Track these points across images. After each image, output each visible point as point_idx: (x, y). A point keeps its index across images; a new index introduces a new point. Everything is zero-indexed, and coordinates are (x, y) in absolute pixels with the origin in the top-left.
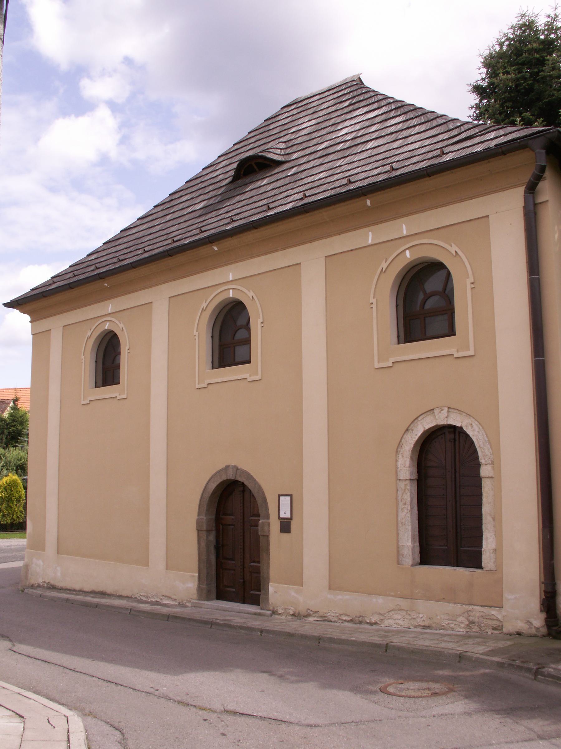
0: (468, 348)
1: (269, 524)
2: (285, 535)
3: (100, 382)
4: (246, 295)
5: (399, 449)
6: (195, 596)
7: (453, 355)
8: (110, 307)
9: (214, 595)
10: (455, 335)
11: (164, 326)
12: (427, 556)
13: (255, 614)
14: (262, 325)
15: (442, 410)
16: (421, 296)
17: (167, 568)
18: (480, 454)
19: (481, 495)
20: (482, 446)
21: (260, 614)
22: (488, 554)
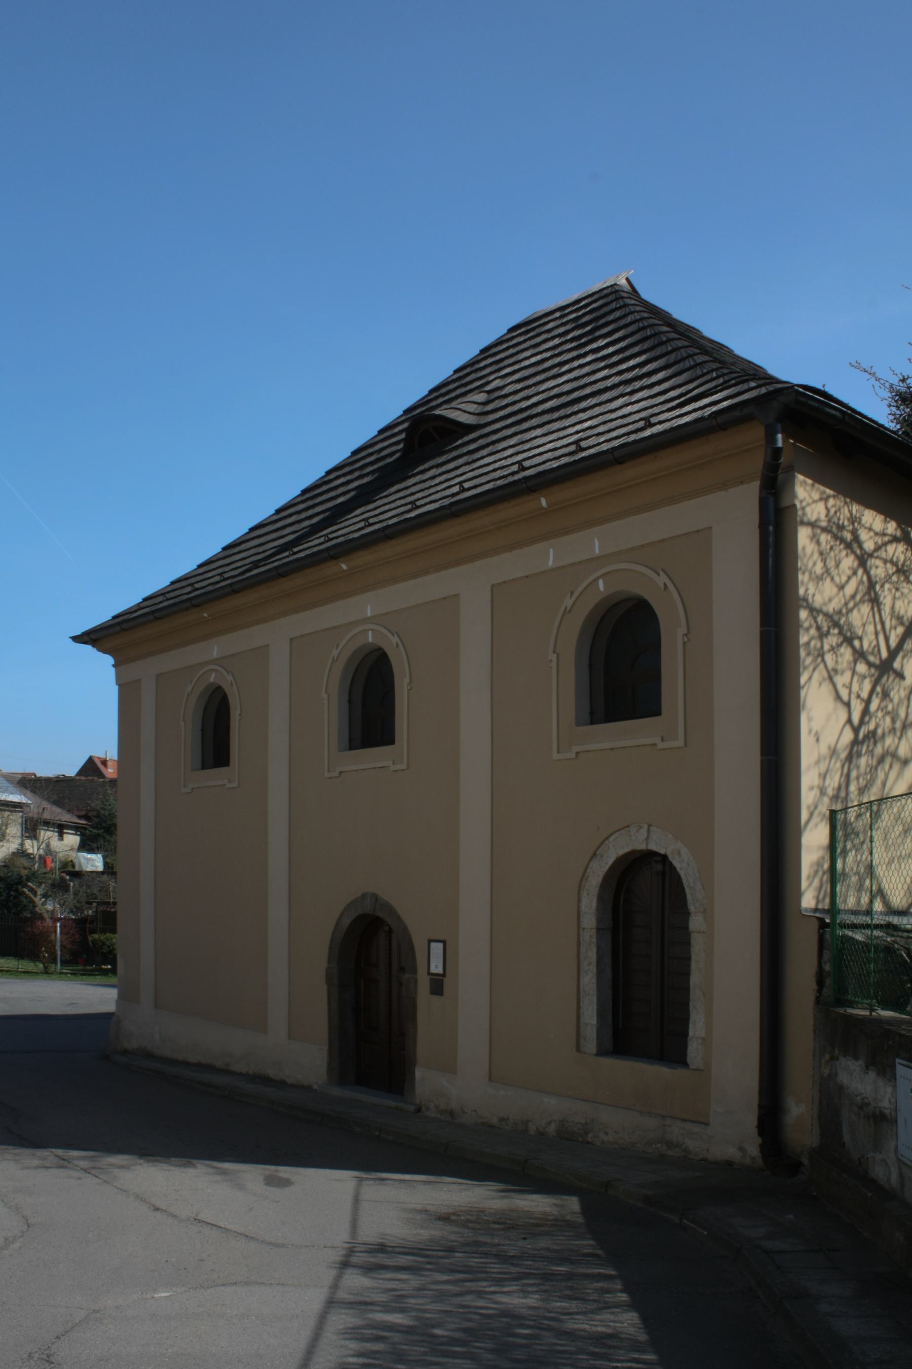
1: (416, 982)
2: (435, 998)
5: (583, 883)
7: (655, 744)
8: (215, 649)
10: (658, 713)
11: (282, 673)
15: (641, 828)
17: (291, 1039)
18: (689, 897)
19: (689, 959)
20: (691, 885)
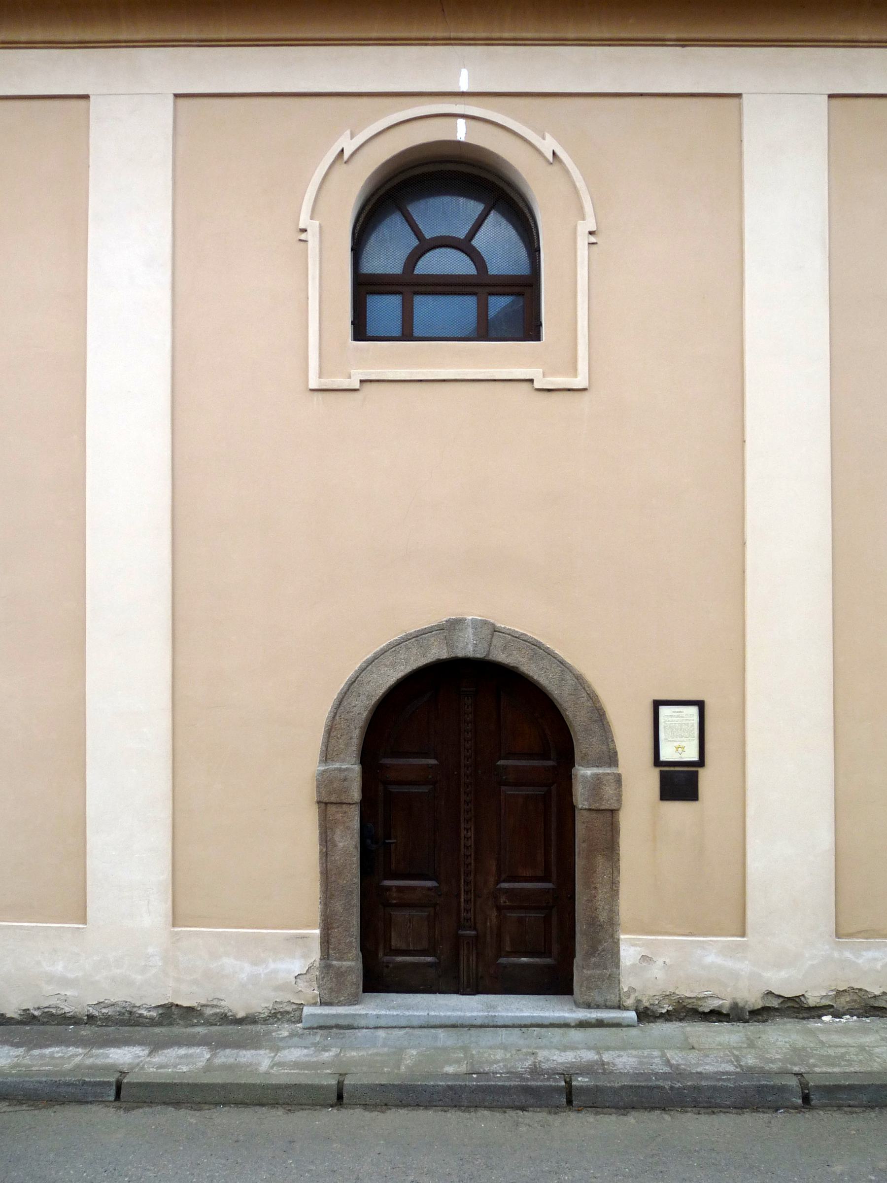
0: (574, 372)
2: (678, 809)
4: (527, 148)
6: (311, 991)
10: (537, 337)
13: (583, 1025)
14: (593, 239)
21: (600, 1024)
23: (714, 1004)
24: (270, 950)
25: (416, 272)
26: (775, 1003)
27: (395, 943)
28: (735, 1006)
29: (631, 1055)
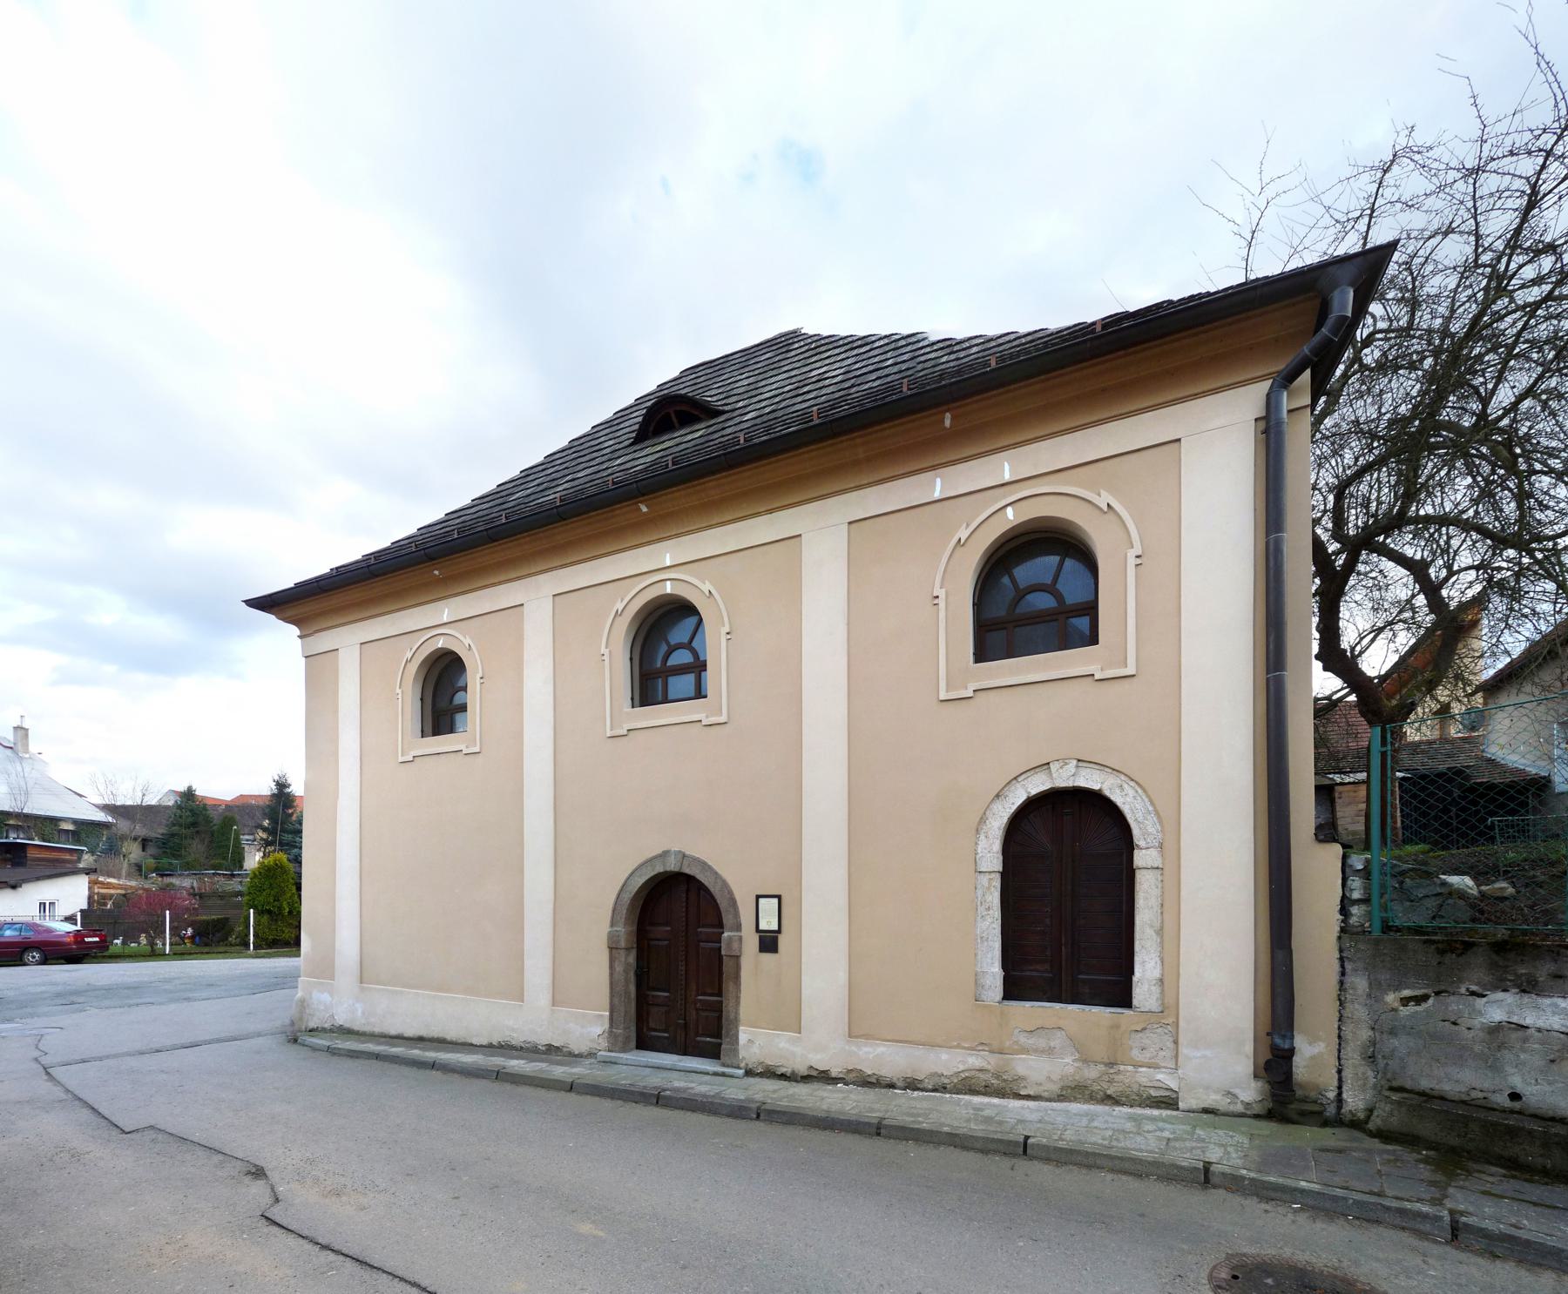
3: (429, 728)
4: (696, 588)
6: (604, 1044)
8: (445, 611)
9: (634, 1043)
11: (545, 637)
12: (1014, 989)
13: (716, 1074)
16: (664, 648)
21: (723, 1075)
22: (1146, 987)
23: (783, 1070)
24: (586, 1024)
25: (1018, 611)
26: (814, 1073)
27: (652, 1025)
28: (793, 1073)
29: (737, 1090)
